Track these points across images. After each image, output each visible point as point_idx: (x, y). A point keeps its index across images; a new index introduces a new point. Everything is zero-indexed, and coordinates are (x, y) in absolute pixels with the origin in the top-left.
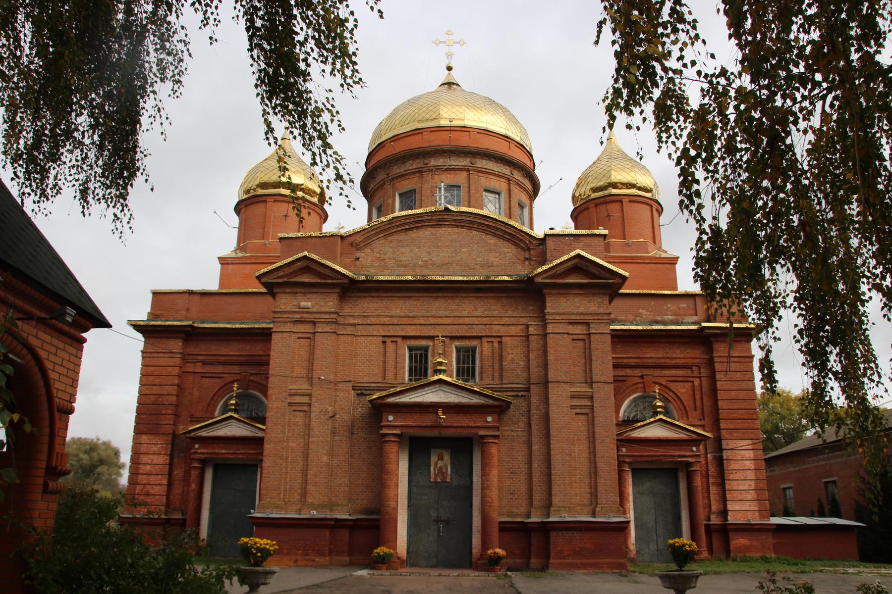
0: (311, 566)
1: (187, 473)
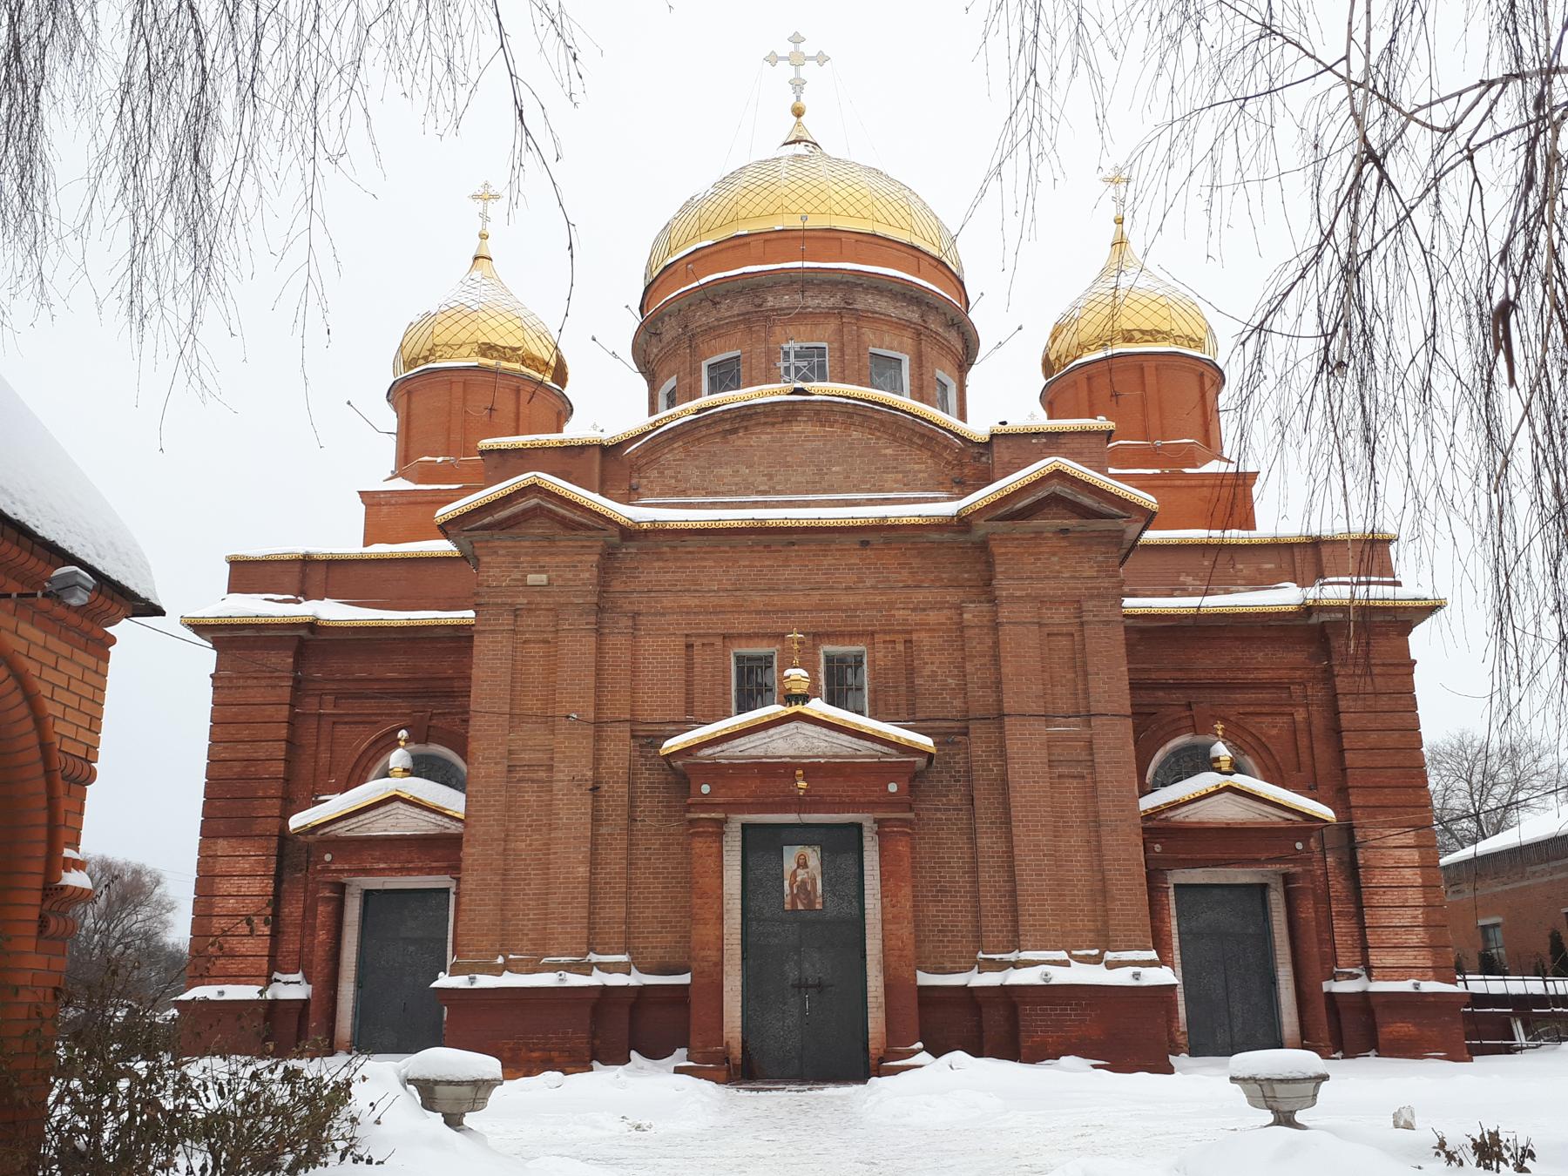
1: (309, 911)
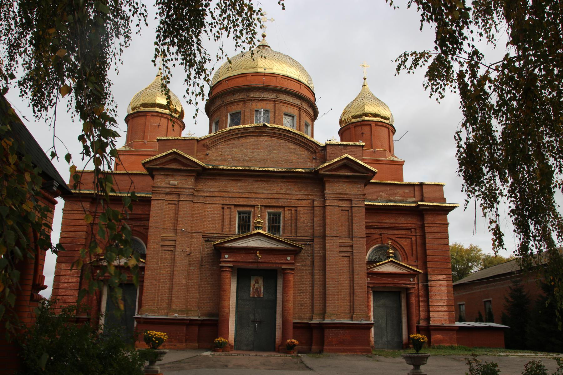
0: (174, 349)
